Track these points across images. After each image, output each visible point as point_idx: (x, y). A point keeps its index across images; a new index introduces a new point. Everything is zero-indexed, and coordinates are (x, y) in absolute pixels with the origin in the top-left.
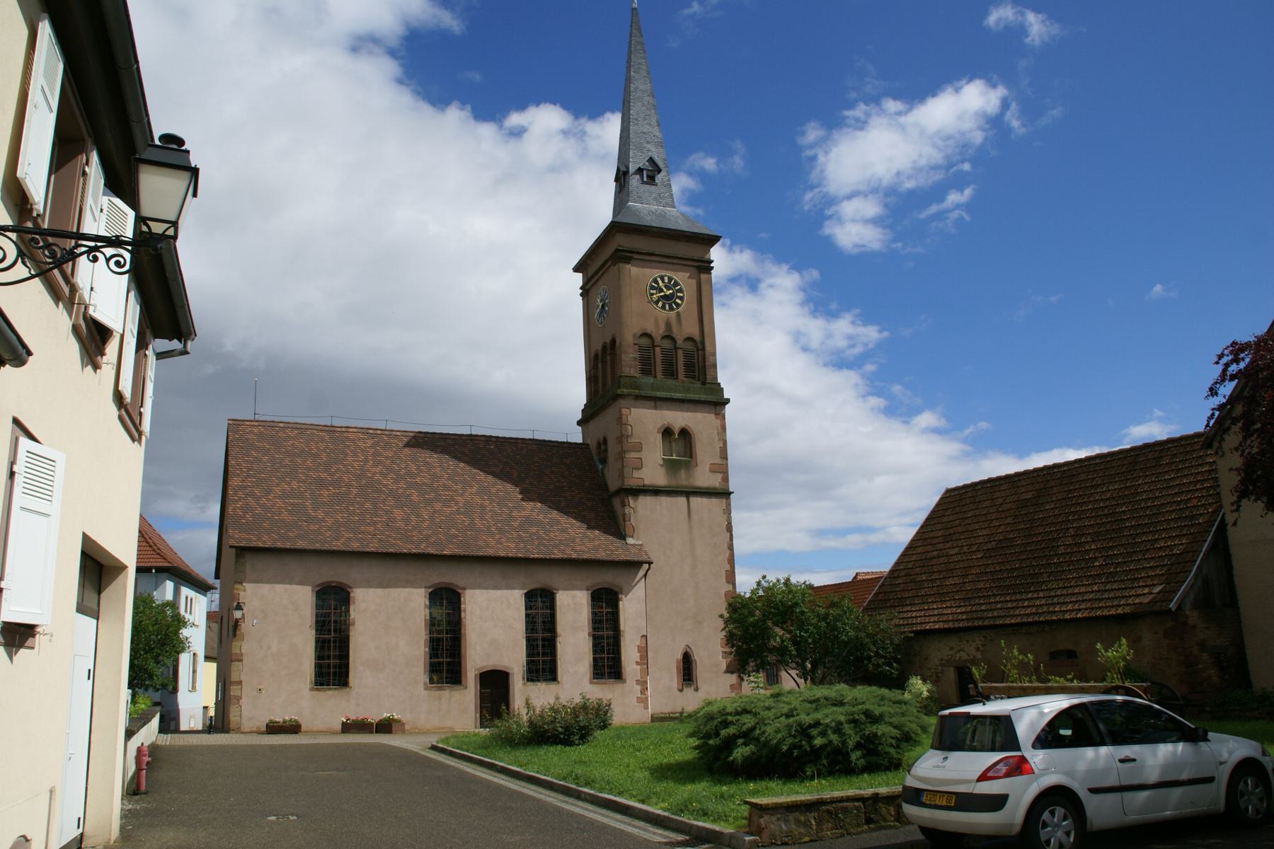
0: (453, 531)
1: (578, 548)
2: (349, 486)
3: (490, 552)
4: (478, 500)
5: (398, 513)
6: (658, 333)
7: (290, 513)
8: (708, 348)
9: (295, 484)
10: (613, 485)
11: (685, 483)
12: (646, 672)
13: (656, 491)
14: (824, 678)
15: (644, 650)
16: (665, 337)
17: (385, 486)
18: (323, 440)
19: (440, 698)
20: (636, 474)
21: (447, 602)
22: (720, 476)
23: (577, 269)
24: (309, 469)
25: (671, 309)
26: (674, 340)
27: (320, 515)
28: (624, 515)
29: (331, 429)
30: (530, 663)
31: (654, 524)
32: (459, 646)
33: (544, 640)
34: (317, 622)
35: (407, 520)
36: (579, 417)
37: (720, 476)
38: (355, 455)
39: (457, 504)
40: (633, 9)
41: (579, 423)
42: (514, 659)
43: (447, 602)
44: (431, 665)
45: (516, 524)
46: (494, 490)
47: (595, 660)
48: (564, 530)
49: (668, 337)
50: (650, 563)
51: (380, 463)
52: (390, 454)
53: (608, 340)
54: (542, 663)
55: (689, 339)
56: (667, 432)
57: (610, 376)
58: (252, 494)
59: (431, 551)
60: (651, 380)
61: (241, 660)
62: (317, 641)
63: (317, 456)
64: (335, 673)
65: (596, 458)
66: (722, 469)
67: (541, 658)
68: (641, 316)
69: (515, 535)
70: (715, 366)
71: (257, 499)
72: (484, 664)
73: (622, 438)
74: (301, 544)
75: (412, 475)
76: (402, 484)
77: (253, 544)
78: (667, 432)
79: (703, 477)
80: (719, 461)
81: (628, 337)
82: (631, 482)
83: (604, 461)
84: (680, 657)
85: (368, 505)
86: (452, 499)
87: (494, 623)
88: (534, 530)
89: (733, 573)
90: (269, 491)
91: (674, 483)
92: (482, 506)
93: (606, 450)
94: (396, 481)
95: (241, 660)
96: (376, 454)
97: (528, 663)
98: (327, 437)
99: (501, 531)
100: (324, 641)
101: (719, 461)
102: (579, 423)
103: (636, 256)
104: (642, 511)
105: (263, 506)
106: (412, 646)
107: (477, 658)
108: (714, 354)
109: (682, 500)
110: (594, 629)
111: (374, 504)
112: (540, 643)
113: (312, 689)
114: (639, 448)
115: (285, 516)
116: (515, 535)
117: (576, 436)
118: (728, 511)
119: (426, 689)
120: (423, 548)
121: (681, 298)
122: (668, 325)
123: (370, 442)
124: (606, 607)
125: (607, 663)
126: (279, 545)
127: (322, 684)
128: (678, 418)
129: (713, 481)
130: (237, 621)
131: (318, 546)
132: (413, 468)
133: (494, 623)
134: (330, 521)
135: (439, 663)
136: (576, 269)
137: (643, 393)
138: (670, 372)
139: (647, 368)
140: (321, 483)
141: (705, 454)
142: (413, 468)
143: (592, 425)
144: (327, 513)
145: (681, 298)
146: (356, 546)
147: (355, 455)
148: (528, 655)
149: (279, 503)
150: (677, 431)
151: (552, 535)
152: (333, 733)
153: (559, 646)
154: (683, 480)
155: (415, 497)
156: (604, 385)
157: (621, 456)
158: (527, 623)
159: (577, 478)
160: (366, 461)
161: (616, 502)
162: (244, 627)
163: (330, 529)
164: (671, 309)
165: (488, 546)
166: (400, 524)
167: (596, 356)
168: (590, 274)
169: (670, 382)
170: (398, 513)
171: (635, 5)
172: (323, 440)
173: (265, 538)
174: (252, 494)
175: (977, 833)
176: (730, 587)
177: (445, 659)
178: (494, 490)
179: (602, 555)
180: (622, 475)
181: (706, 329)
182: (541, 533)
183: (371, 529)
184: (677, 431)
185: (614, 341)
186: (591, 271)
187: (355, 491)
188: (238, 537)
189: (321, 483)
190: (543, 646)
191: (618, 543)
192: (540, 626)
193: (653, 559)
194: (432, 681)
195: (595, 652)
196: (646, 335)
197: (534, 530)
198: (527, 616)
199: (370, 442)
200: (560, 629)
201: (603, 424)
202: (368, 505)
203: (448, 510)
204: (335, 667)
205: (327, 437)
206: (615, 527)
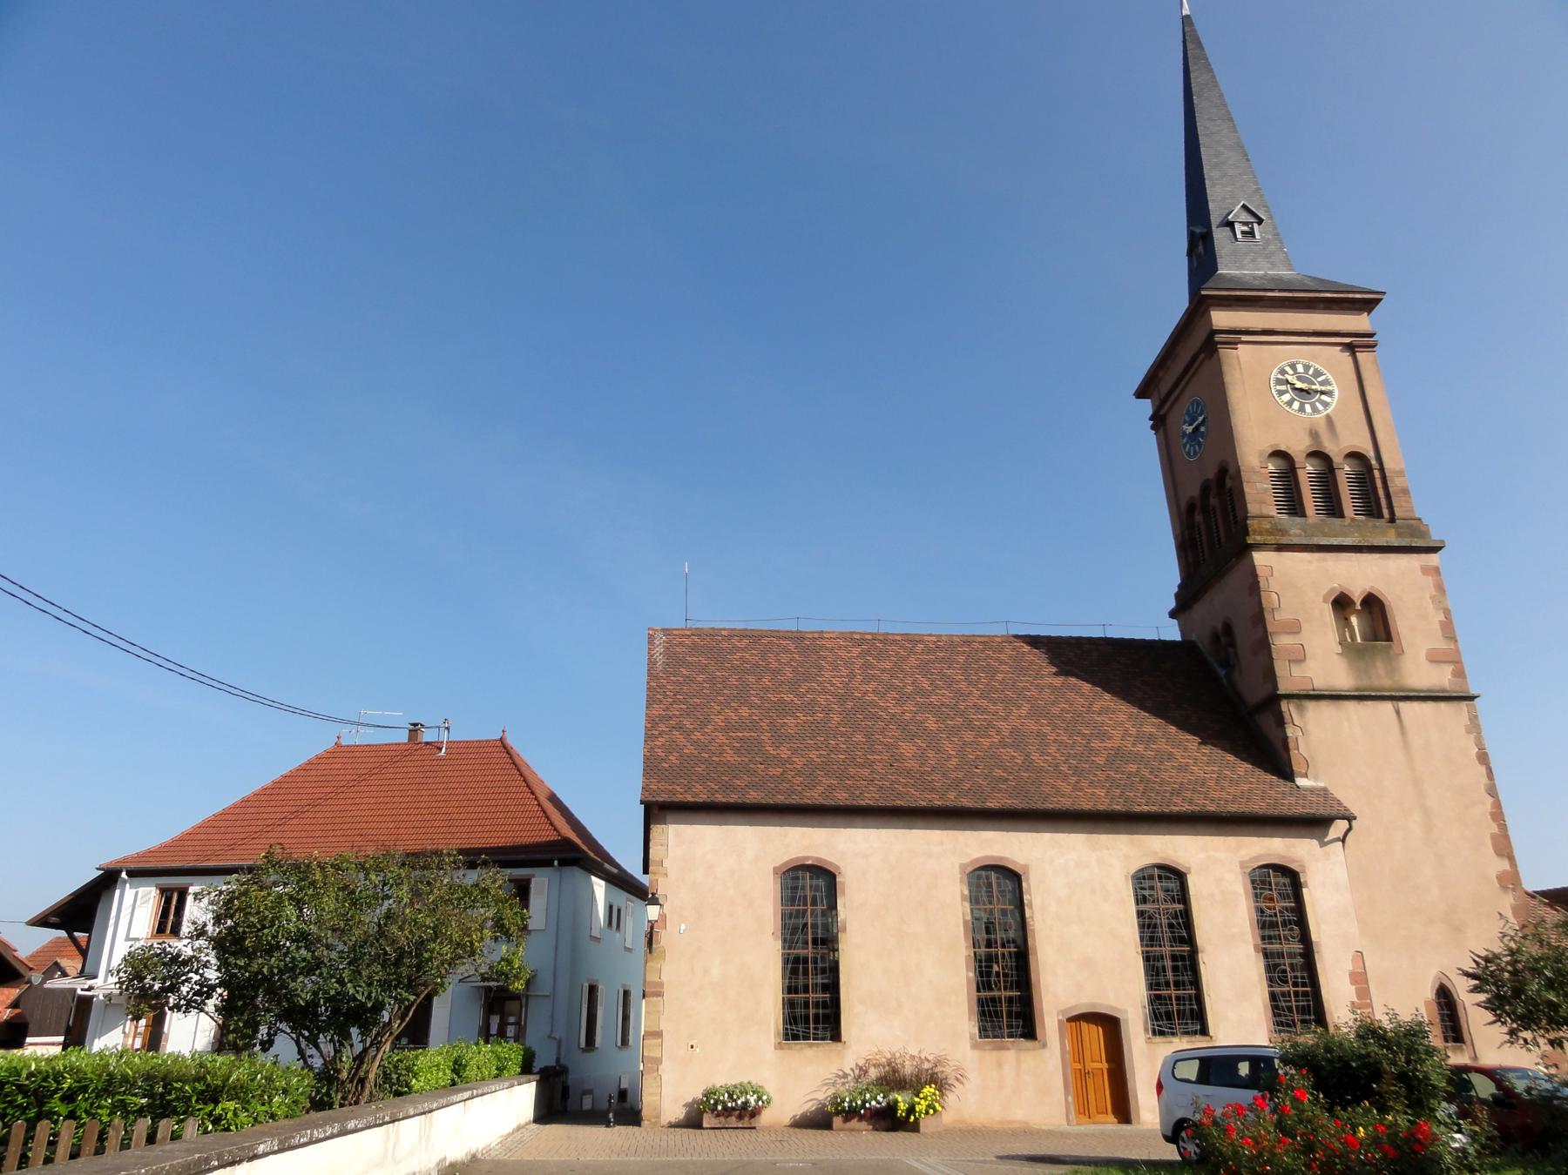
0: (999, 773)
1: (1216, 795)
2: (828, 711)
4: (1032, 726)
5: (907, 749)
6: (1298, 446)
7: (738, 751)
9: (745, 712)
17: (885, 709)
18: (788, 651)
19: (1000, 1065)
20: (1297, 671)
22: (1448, 670)
24: (766, 690)
27: (785, 752)
29: (798, 637)
30: (1155, 1000)
33: (1174, 958)
34: (784, 926)
35: (922, 758)
36: (1172, 604)
37: (1448, 670)
38: (836, 668)
39: (998, 732)
40: (1186, 20)
41: (1173, 614)
42: (1128, 995)
44: (981, 1003)
45: (1100, 760)
46: (1055, 710)
48: (1183, 768)
49: (1318, 455)
50: (1350, 818)
51: (873, 678)
52: (888, 665)
53: (1211, 474)
55: (1354, 456)
56: (1341, 603)
58: (679, 727)
59: (967, 803)
61: (660, 994)
62: (786, 961)
63: (776, 672)
64: (816, 1016)
65: (1211, 659)
67: (1173, 992)
71: (688, 734)
72: (1073, 1002)
74: (753, 797)
75: (921, 692)
76: (909, 706)
77: (679, 798)
78: (1341, 603)
80: (1442, 644)
82: (1281, 691)
83: (1227, 664)
85: (859, 738)
86: (989, 726)
88: (1133, 768)
89: (1506, 837)
90: (703, 725)
91: (1365, 682)
92: (1041, 735)
93: (1232, 644)
94: (899, 702)
95: (660, 994)
96: (867, 666)
98: (792, 647)
99: (1077, 771)
100: (797, 960)
101: (1442, 644)
102: (1173, 614)
103: (1244, 338)
104: (1315, 734)
105: (695, 743)
106: (947, 977)
107: (1059, 988)
109: (1387, 707)
111: (868, 736)
112: (1168, 963)
113: (779, 1046)
114: (1294, 628)
115: (730, 756)
116: (1102, 776)
117: (1171, 632)
119: (975, 1046)
120: (952, 799)
122: (1314, 435)
123: (856, 651)
126: (720, 798)
127: (795, 1037)
128: (1360, 574)
129: (1441, 678)
130: (652, 924)
131: (780, 799)
132: (926, 685)
134: (799, 762)
135: (993, 1000)
136: (1141, 393)
137: (1284, 540)
138: (1333, 507)
139: (1294, 505)
140: (784, 709)
142: (926, 685)
143: (1198, 611)
144: (794, 751)
146: (842, 798)
147: (836, 668)
148: (1151, 987)
149: (721, 738)
150: (1358, 601)
151: (1165, 776)
154: (1381, 678)
155: (931, 724)
158: (1142, 927)
160: (852, 676)
162: (664, 938)
163: (799, 773)
164: (1315, 410)
165: (1058, 792)
166: (912, 764)
167: (1191, 508)
169: (1337, 521)
170: (907, 749)
171: (1186, 11)
172: (788, 651)
173: (698, 788)
174: (679, 727)
176: (1505, 865)
177: (1006, 996)
178: (1055, 710)
179: (1258, 807)
182: (1146, 773)
183: (866, 772)
184: (1357, 598)
187: (837, 718)
189: (784, 709)
190: (1175, 969)
191: (1281, 785)
192: (1165, 933)
193: (1354, 811)
194: (984, 1032)
197: (1133, 768)
198: (1140, 914)
199: (856, 651)
201: (1211, 610)
202: (859, 738)
203: (986, 742)
204: (817, 1005)
205: (792, 647)
206: (1274, 758)
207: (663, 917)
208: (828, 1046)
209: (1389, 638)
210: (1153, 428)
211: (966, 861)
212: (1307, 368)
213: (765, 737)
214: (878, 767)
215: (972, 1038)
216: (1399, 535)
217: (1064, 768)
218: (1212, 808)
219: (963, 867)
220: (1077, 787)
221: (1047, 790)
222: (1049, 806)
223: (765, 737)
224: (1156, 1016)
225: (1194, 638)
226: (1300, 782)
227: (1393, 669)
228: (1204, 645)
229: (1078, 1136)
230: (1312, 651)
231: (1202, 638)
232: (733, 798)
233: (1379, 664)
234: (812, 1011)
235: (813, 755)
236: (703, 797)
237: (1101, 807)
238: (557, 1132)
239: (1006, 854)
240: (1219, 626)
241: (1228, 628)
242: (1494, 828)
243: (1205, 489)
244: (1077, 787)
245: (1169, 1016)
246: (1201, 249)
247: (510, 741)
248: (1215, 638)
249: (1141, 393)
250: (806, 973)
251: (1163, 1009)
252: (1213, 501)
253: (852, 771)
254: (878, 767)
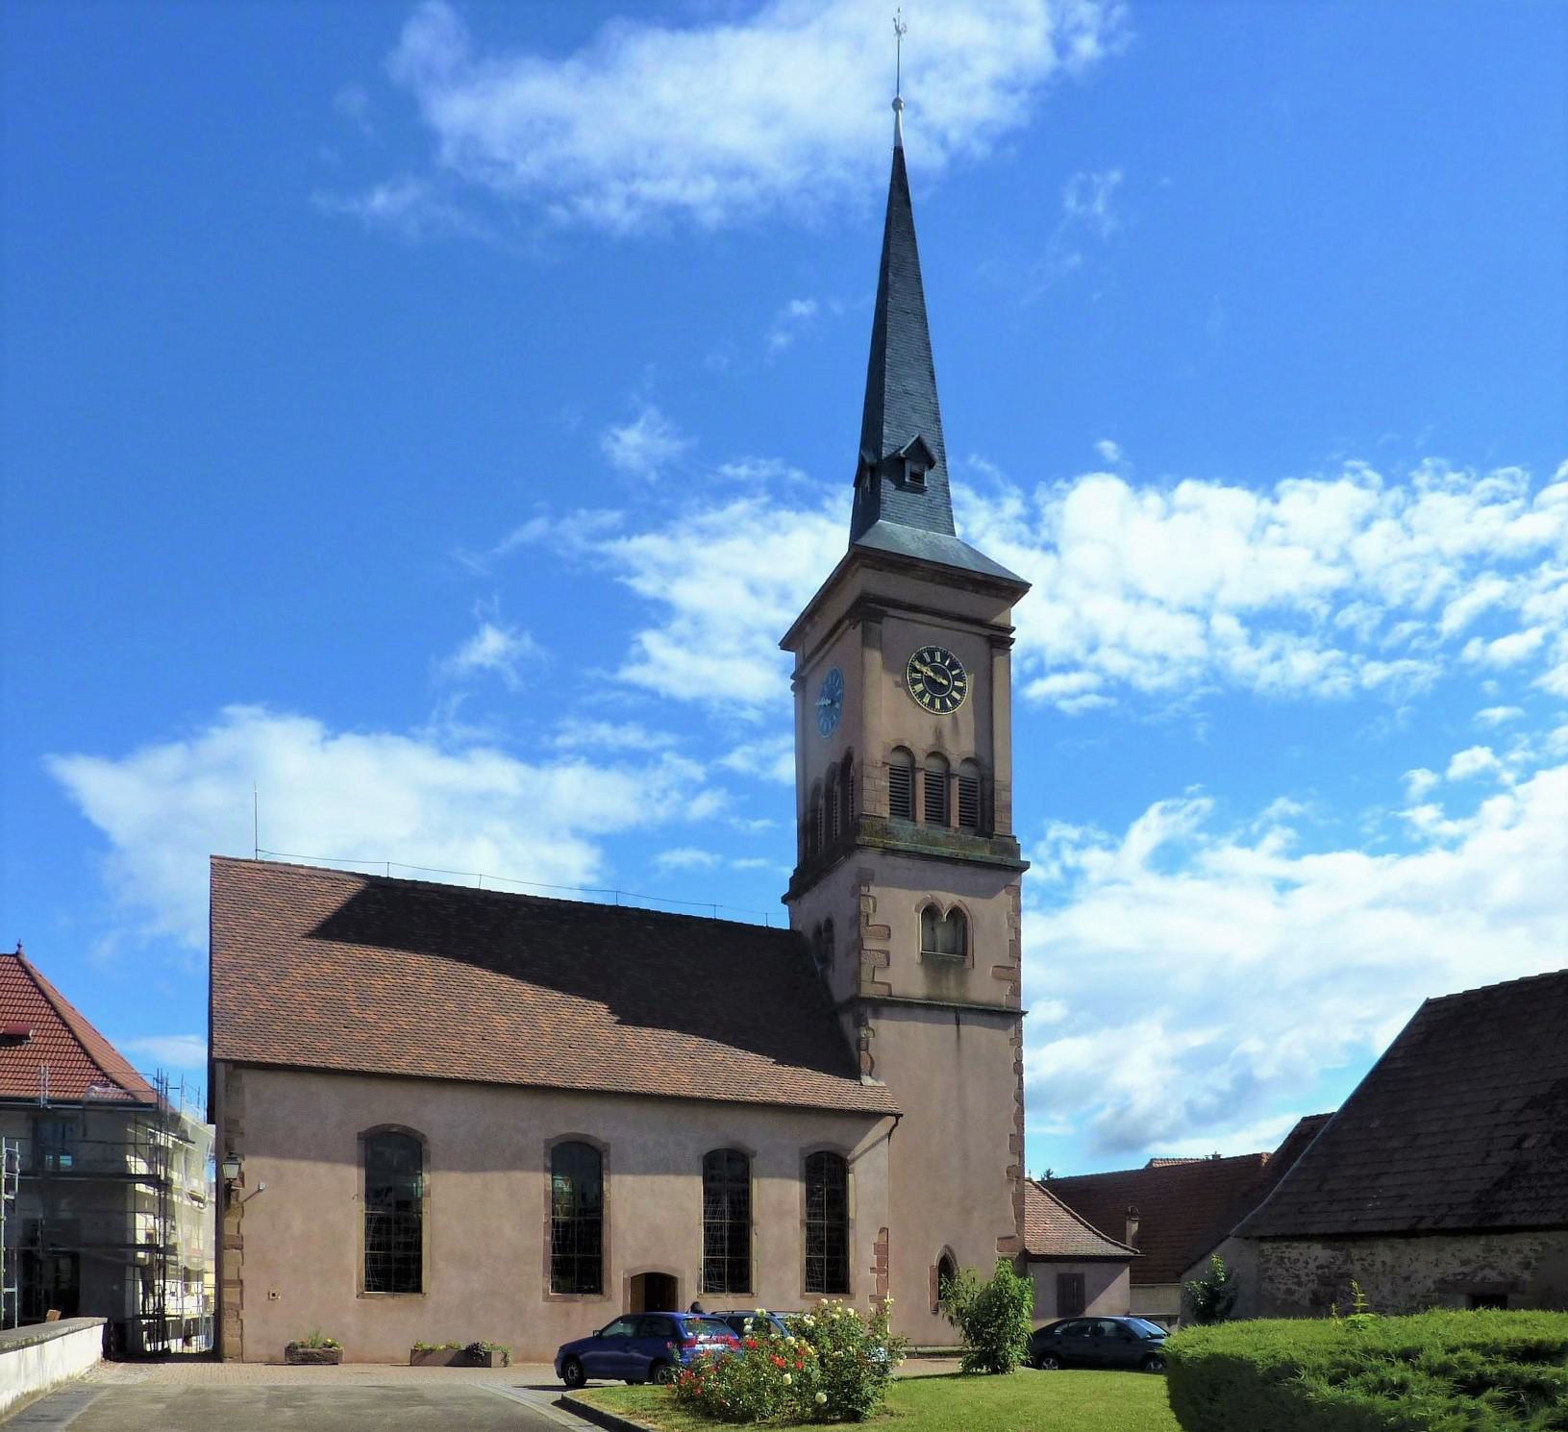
3: (650, 1087)
5: (501, 1022)
8: (999, 776)
10: (840, 992)
11: (953, 993)
12: (884, 1284)
13: (906, 1006)
14: (407, 1231)
15: (882, 1250)
16: (933, 754)
19: (568, 1314)
21: (581, 1166)
23: (786, 644)
25: (944, 708)
26: (945, 760)
28: (859, 1040)
31: (902, 1055)
32: (599, 1234)
36: (786, 889)
37: (1008, 987)
41: (785, 900)
42: (686, 1258)
43: (581, 1166)
47: (809, 1262)
54: (730, 1261)
56: (930, 912)
57: (831, 829)
60: (909, 826)
62: (369, 1219)
66: (1010, 973)
68: (895, 717)
69: (689, 1064)
70: (1009, 807)
73: (857, 919)
74: (337, 1061)
79: (982, 988)
81: (876, 750)
82: (868, 990)
84: (936, 1263)
87: (655, 1218)
93: (831, 940)
97: (708, 1263)
102: (785, 900)
104: (885, 1035)
108: (1008, 788)
110: (809, 1215)
116: (689, 1064)
117: (780, 919)
118: (1017, 1041)
120: (541, 1077)
121: (961, 691)
122: (938, 734)
124: (827, 1180)
125: (828, 1268)
126: (300, 1061)
131: (366, 1066)
133: (655, 1218)
138: (938, 814)
139: (902, 805)
141: (985, 953)
143: (808, 900)
145: (961, 691)
146: (430, 1069)
148: (707, 1252)
149: (301, 996)
152: (394, 1362)
153: (754, 1239)
154: (950, 990)
156: (829, 836)
157: (858, 947)
159: (780, 989)
161: (846, 1021)
167: (816, 789)
168: (808, 651)
169: (940, 832)
170: (501, 1022)
175: (605, 1240)
180: (856, 978)
181: (998, 744)
185: (848, 759)
186: (811, 644)
187: (428, 983)
188: (233, 1047)
195: (810, 1250)
196: (900, 749)
200: (756, 1213)
202: (451, 1006)
204: (398, 1261)
206: (846, 1063)
207: (242, 1176)
208: (415, 1296)
209: (965, 953)
210: (793, 688)
211: (551, 1136)
212: (944, 657)
213: (351, 997)
214: (469, 1039)
215: (545, 1291)
216: (993, 852)
217: (655, 1052)
218: (782, 1099)
219: (547, 1142)
220: (663, 1072)
221: (636, 1073)
222: (635, 1089)
223: (351, 997)
224: (708, 1276)
225: (799, 928)
226: (867, 1081)
227: (962, 982)
228: (809, 934)
229: (120, 1391)
230: (899, 961)
231: (807, 928)
232: (315, 1062)
233: (952, 977)
234: (394, 1266)
235: (402, 1021)
236: (281, 1060)
237: (682, 1093)
238: (120, 1367)
239: (591, 1133)
240: (822, 921)
241: (829, 924)
242: (1015, 1131)
243: (832, 773)
244: (663, 1072)
245: (720, 1277)
246: (868, 484)
247: (28, 958)
248: (818, 931)
249: (786, 644)
250: (388, 1232)
251: (715, 1271)
252: (837, 788)
253: (442, 1042)
254: (469, 1039)
